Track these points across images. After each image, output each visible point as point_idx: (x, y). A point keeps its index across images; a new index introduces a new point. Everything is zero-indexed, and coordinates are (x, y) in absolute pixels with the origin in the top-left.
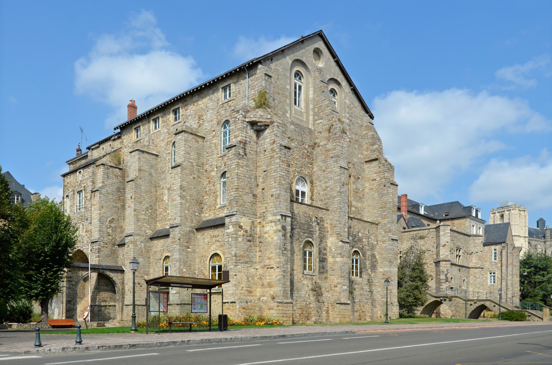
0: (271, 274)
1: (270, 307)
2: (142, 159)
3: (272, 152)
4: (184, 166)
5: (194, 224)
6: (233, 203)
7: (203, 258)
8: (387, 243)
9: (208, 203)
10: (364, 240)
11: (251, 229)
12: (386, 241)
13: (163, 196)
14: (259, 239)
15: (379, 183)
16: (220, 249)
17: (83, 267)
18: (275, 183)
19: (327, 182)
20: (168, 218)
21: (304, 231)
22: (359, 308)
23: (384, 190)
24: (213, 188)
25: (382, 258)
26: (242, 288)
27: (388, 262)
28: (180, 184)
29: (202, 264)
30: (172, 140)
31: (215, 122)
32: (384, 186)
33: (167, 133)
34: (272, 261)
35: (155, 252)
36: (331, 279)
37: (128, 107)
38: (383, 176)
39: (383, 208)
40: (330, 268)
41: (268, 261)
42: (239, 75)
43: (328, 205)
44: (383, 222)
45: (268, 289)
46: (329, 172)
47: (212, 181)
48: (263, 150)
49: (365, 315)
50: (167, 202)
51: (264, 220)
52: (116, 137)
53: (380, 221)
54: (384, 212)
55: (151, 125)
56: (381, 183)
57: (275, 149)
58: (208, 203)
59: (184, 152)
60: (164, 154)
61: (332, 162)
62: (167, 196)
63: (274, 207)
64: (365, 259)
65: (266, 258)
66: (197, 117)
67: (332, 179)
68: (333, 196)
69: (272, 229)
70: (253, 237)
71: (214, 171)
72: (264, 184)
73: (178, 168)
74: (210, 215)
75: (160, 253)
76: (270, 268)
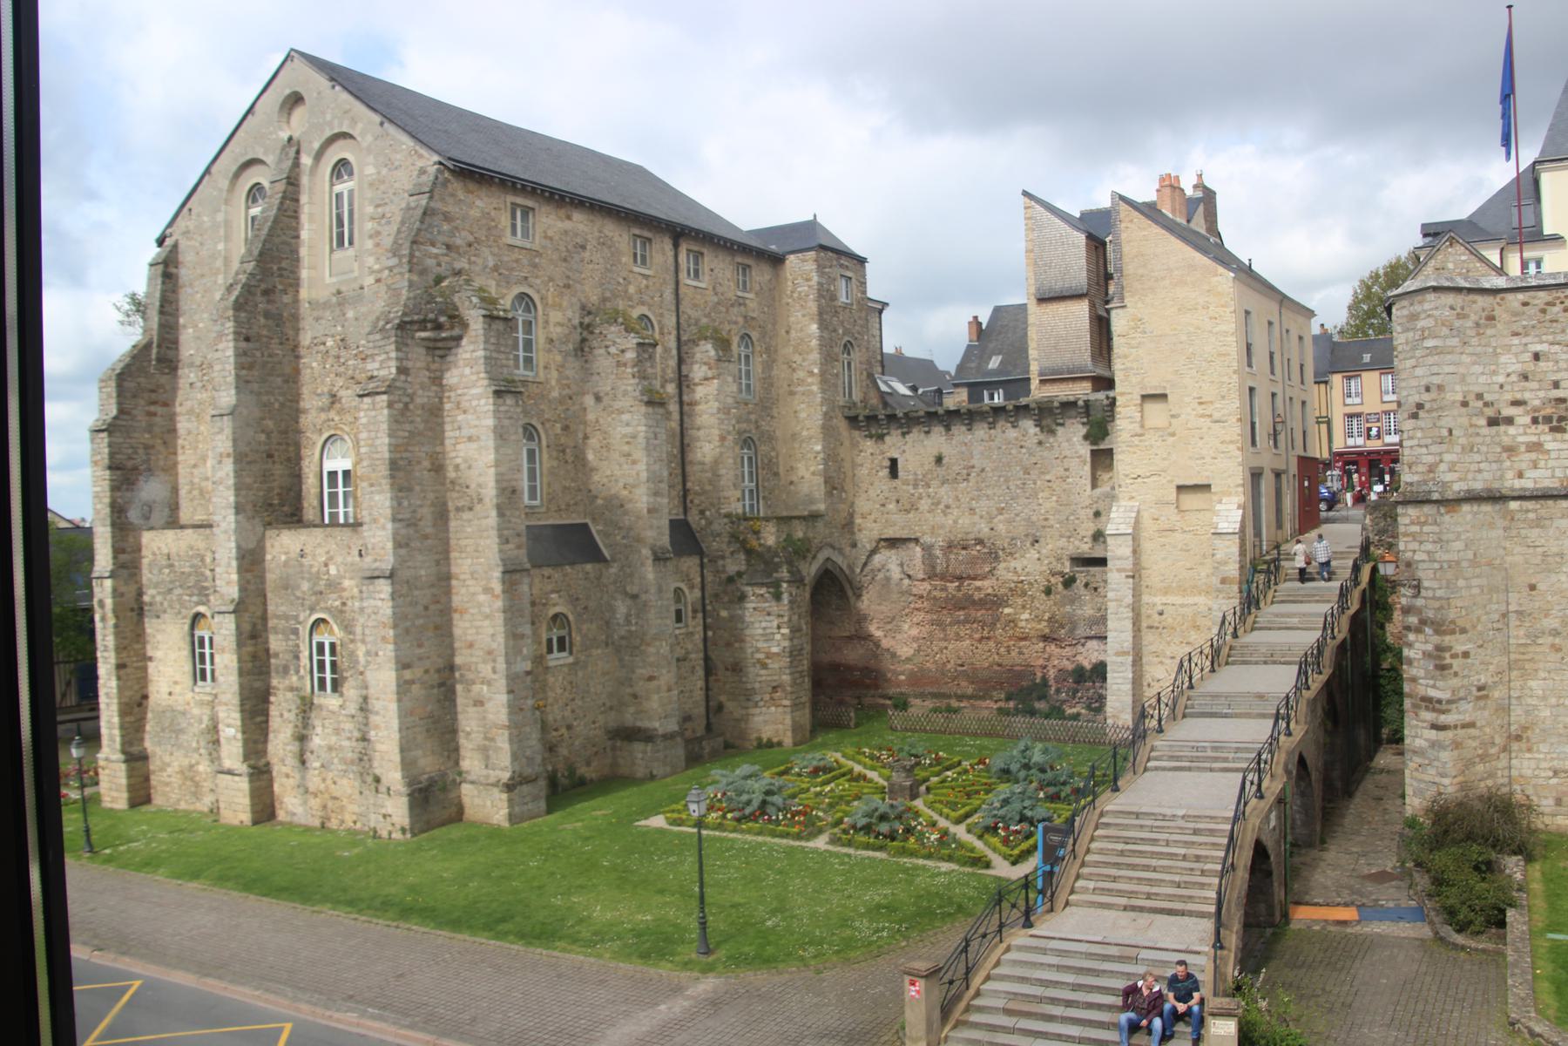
10: (347, 583)
21: (188, 592)
22: (322, 787)
49: (342, 808)
64: (352, 641)
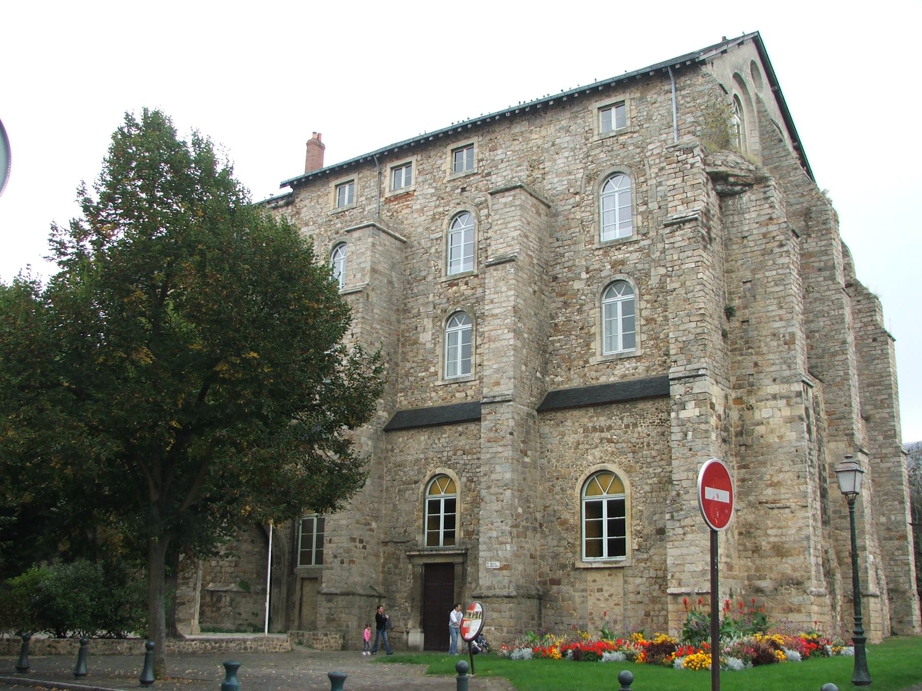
0: (783, 523)
1: (789, 604)
2: (377, 247)
3: (765, 241)
4: (519, 263)
6: (694, 349)
7: (560, 482)
8: (891, 460)
9: (561, 352)
12: (889, 456)
13: (418, 333)
14: (739, 438)
15: (860, 334)
16: (617, 460)
18: (781, 308)
19: (812, 321)
20: (432, 385)
23: (873, 349)
24: (578, 318)
25: (881, 494)
27: (897, 503)
28: (512, 303)
29: (558, 497)
30: (447, 211)
31: (580, 175)
32: (875, 340)
33: (432, 195)
34: (783, 490)
35: (399, 465)
36: (839, 537)
37: (308, 144)
38: (870, 319)
39: (874, 386)
40: (835, 512)
41: (769, 491)
42: (648, 84)
43: (819, 370)
44: (877, 416)
45: (775, 560)
46: (815, 300)
47: (574, 301)
48: (739, 235)
50: (429, 346)
51: (750, 392)
52: (281, 203)
53: (871, 412)
54: (878, 394)
55: (388, 178)
56: (866, 334)
57: (774, 234)
58: (561, 352)
59: (519, 232)
60: (423, 241)
61: (822, 279)
62: (430, 333)
63: (781, 363)
65: (761, 485)
66: (526, 164)
67: (826, 315)
68: (832, 350)
69: (778, 414)
71: (580, 279)
72: (746, 311)
73: (508, 265)
74: (569, 379)
75: (416, 468)
76: (779, 508)
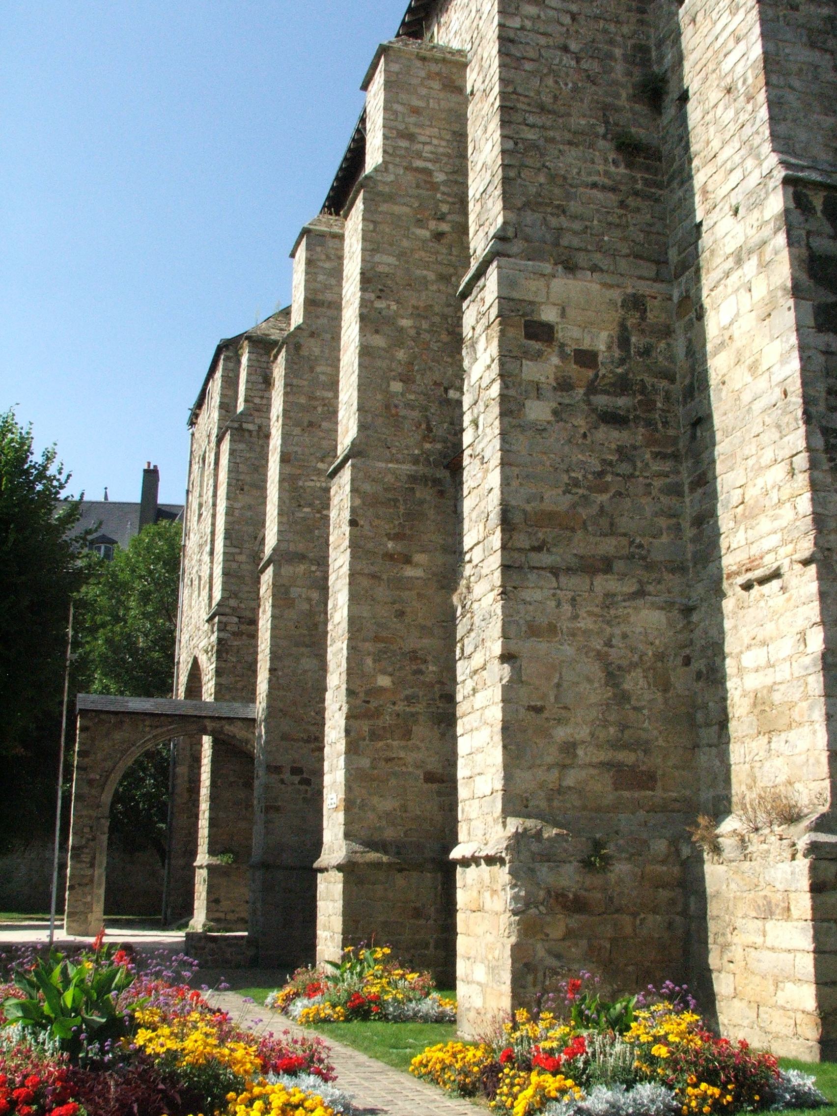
5: (439, 446)
11: (624, 342)
17: (133, 713)
26: (569, 748)
70: (643, 392)
76: (762, 581)
